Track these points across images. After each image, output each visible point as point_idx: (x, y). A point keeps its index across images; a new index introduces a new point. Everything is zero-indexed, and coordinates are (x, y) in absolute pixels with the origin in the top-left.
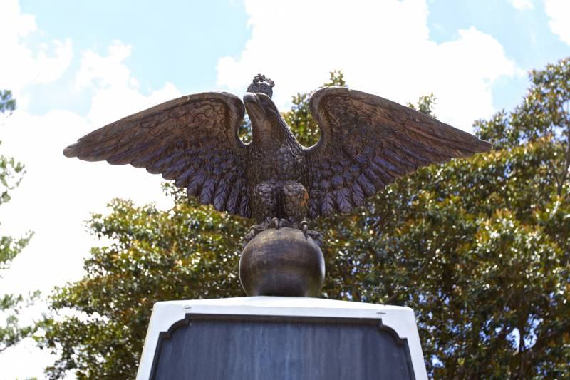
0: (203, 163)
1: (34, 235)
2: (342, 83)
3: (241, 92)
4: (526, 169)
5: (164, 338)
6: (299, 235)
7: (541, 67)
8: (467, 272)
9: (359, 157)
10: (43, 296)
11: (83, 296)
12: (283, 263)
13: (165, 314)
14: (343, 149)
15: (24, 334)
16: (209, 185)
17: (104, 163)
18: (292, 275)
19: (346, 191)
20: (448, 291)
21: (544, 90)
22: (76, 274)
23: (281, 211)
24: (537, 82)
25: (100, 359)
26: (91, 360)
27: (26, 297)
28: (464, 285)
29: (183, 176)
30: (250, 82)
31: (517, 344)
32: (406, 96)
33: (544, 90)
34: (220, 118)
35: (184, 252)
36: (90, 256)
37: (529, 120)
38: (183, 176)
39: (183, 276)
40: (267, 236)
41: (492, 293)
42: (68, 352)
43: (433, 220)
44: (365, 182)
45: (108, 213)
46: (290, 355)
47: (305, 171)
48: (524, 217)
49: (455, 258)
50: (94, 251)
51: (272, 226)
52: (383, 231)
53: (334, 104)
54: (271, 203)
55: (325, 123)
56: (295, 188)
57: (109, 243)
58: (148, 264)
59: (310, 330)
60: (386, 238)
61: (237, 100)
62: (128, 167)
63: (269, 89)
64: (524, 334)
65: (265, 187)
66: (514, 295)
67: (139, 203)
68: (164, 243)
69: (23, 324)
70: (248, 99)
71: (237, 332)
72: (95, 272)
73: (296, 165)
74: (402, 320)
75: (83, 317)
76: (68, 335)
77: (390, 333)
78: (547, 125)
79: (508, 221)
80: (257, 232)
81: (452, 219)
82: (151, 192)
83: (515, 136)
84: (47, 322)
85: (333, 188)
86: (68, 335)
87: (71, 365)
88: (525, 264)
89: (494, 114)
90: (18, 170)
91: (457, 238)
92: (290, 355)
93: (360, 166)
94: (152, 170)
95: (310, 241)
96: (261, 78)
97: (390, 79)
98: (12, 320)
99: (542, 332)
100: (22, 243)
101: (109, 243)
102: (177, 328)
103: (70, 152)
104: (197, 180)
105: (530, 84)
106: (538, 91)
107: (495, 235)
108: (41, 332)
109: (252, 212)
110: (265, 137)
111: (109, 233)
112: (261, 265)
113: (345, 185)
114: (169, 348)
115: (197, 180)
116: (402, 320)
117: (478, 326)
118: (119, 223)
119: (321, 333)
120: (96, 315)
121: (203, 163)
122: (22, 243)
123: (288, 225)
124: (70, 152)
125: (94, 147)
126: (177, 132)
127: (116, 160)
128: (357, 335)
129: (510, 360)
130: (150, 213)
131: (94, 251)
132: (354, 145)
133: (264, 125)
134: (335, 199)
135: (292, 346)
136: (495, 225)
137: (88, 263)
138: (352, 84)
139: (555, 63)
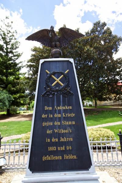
0: (45, 40)
1: (17, 31)
2: (65, 27)
3: (49, 29)
4: (92, 39)
5: (42, 64)
6: (58, 50)
7: (95, 22)
8: (83, 55)
9: (66, 38)
10: (26, 61)
11: (31, 61)
12: (56, 54)
13: (42, 61)
14: (64, 37)
15: (24, 66)
16: (46, 43)
17: (31, 41)
18: (58, 55)
19: (65, 43)
20: (81, 58)
21: (95, 26)
22: (30, 58)
23: (56, 46)
24: (94, 25)
25: (35, 69)
26: (34, 70)
27: (23, 61)
28: (83, 57)
29: (42, 42)
30: (50, 27)
31: (89, 64)
32: (74, 29)
33: (95, 26)
34: (46, 33)
35: (45, 53)
36: (31, 55)
37: (93, 31)
38: (42, 42)
39: (44, 57)
40: (54, 50)
41: (86, 58)
42: (30, 69)
43: (79, 47)
44: (67, 42)
45: (33, 48)
46: (58, 65)
47: (59, 40)
48: (91, 46)
49: (82, 53)
50: (32, 54)
51: (55, 49)
52: (72, 49)
53: (63, 30)
54: (54, 45)
55: (62, 33)
56: (58, 43)
57: (34, 53)
58: (40, 56)
59: (60, 62)
60: (72, 50)
61: (49, 30)
62: (34, 41)
63: (53, 28)
64: (91, 63)
65: (54, 43)
66: (89, 57)
67: (38, 46)
68: (42, 52)
69: (24, 65)
70: (50, 30)
71: (51, 63)
72: (32, 57)
73: (58, 40)
74: (72, 60)
75: (32, 64)
76: (30, 66)
77: (70, 62)
78: (96, 32)
79: (88, 47)
80: (53, 49)
81: (81, 47)
82: (38, 45)
83: (91, 34)
84: (27, 65)
85: (63, 43)
86: (30, 66)
87: (31, 70)
88: (91, 53)
89: (87, 31)
90: (19, 43)
91: (82, 49)
92: (58, 65)
93: (67, 39)
94: (38, 41)
95: (60, 50)
96: (52, 26)
97: (72, 27)
98: (22, 65)
99: (93, 62)
100: (22, 54)
101: (34, 53)
102: (43, 63)
103: (26, 39)
104: (44, 43)
105: (93, 25)
106: (95, 26)
107: (87, 49)
108: (26, 66)
109: (52, 47)
110: (53, 35)
111: (34, 51)
112: (54, 54)
113: (65, 42)
114: (42, 65)
115: (44, 43)
116: (72, 60)
117: (84, 62)
118: (35, 50)
119: (61, 62)
120: (33, 63)
121: (45, 40)
122: (22, 54)
123: (57, 48)
124: (26, 39)
125: (29, 38)
126: (41, 35)
127: (33, 40)
128: (66, 62)
129: (89, 66)
130: (39, 48)
131: (32, 54)
132: (66, 36)
133: (53, 34)
134: (63, 44)
135: (58, 64)
136: (87, 48)
137: (31, 56)
138: (67, 27)
139: (97, 21)
